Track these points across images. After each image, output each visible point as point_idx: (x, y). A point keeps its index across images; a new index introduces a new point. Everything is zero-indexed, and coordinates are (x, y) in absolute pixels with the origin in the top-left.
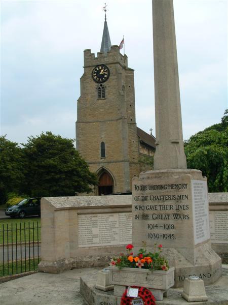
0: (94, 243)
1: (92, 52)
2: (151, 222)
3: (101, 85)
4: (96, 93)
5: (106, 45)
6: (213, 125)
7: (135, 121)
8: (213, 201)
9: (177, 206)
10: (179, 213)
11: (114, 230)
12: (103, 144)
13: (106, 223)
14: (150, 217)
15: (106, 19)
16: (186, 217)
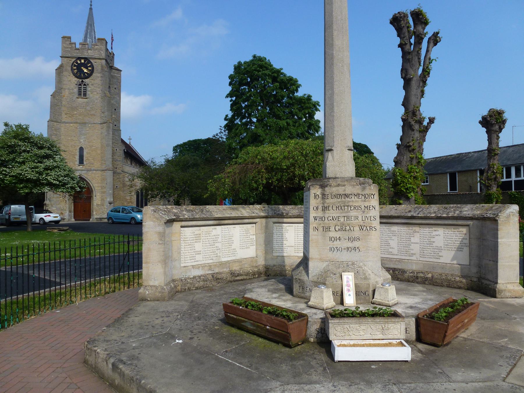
0: (197, 261)
1: (73, 41)
2: (333, 234)
3: (82, 81)
4: (76, 90)
5: (90, 35)
6: (186, 140)
7: (119, 127)
8: (384, 214)
9: (364, 217)
10: (365, 224)
11: (217, 245)
12: (81, 149)
13: (209, 237)
14: (332, 229)
15: (91, 5)
16: (373, 229)
